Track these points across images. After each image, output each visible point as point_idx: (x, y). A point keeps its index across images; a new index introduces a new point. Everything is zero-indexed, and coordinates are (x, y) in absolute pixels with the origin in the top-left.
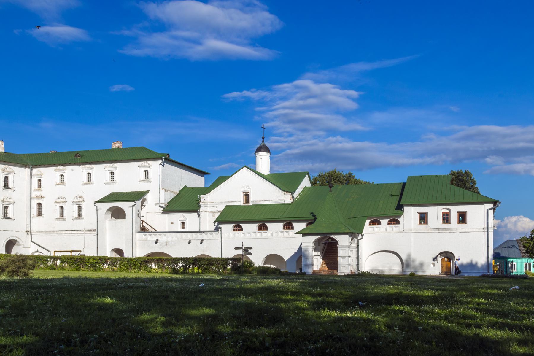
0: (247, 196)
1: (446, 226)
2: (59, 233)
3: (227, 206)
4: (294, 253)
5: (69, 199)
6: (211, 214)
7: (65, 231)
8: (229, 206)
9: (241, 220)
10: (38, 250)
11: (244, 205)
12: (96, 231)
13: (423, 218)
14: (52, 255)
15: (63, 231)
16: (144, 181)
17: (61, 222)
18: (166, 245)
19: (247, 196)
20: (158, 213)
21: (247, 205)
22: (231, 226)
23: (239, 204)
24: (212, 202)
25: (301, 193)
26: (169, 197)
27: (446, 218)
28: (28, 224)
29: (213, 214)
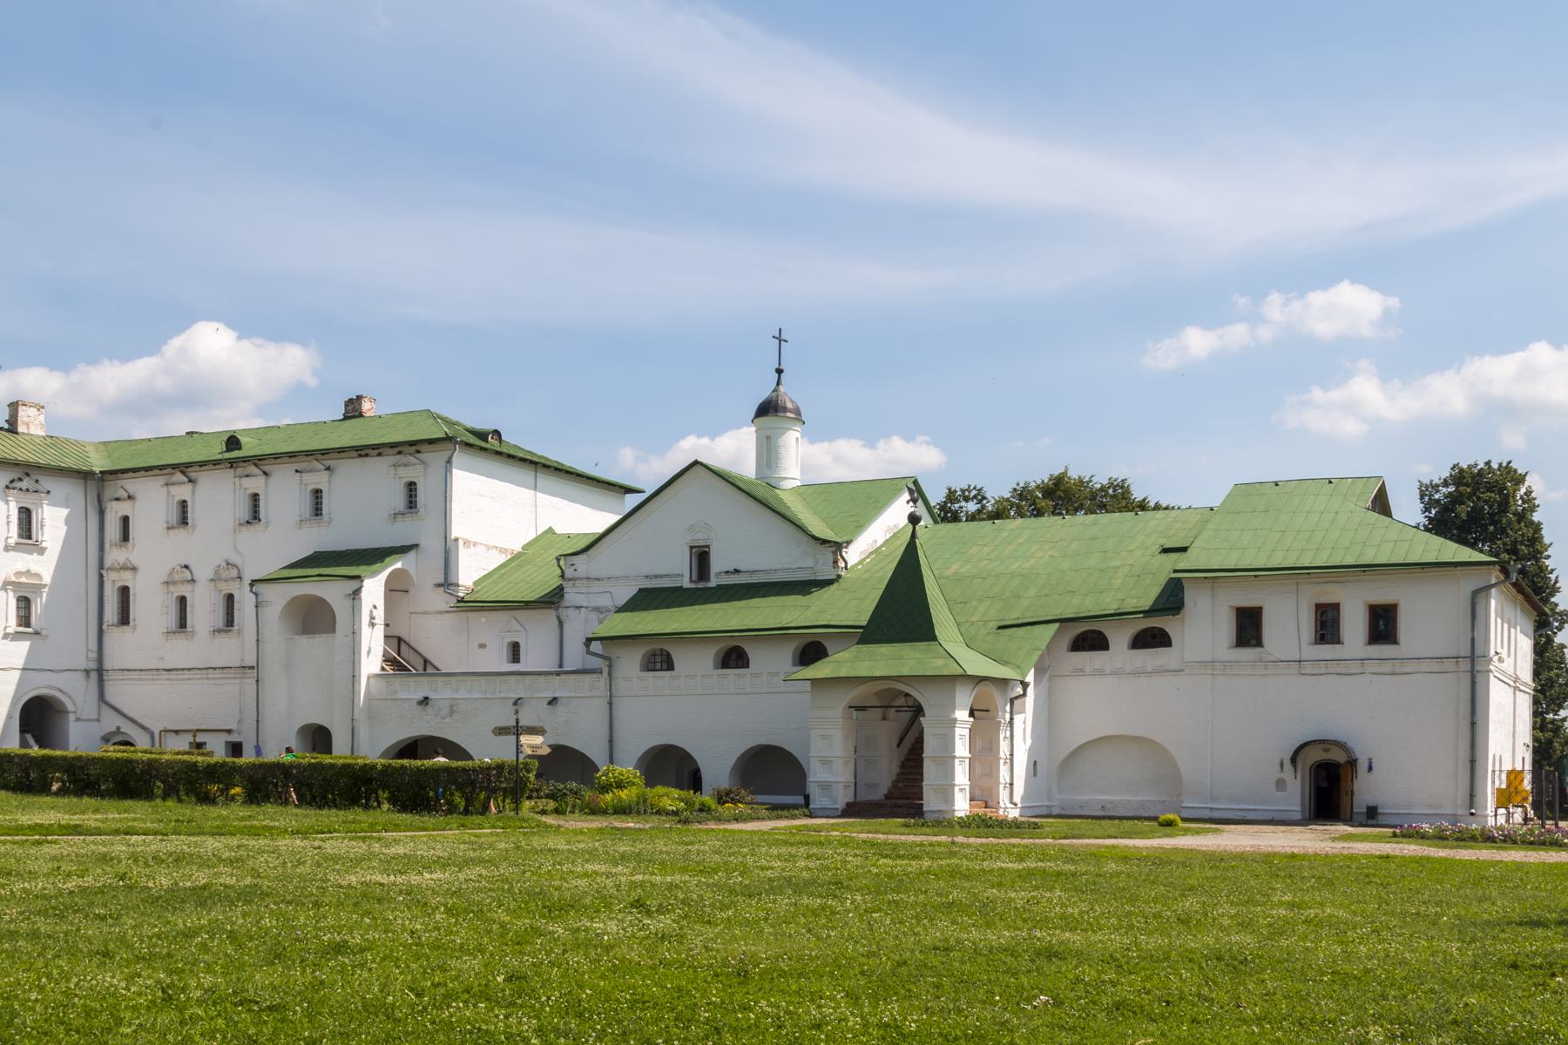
0: (701, 558)
1: (1326, 651)
2: (173, 675)
3: (641, 590)
5: (203, 572)
7: (189, 669)
8: (670, 588)
10: (118, 728)
11: (693, 586)
12: (255, 671)
13: (1249, 627)
15: (183, 669)
16: (403, 514)
17: (179, 642)
18: (452, 712)
20: (440, 612)
21: (700, 585)
23: (679, 585)
25: (882, 546)
26: (1308, 562)
27: (1327, 625)
28: (91, 651)
29: (601, 616)
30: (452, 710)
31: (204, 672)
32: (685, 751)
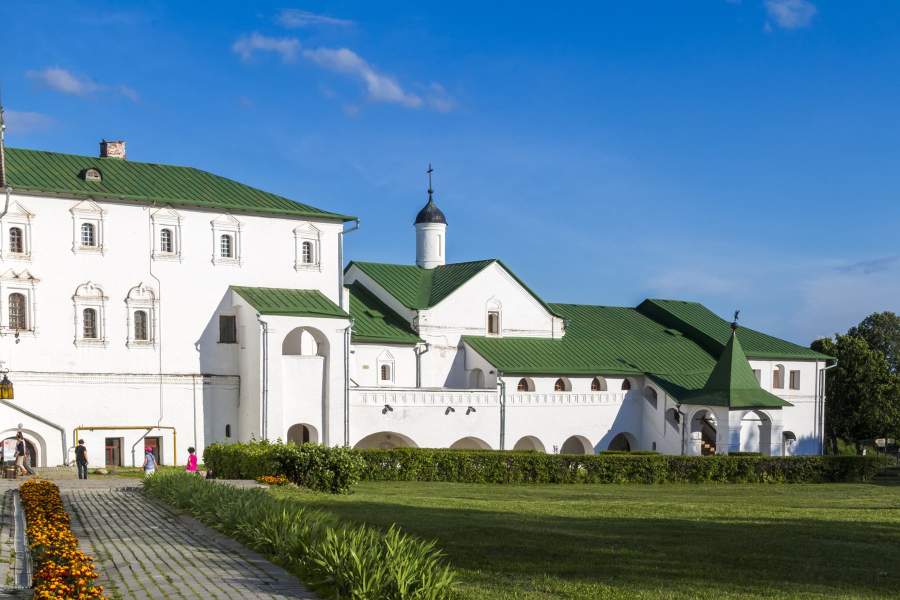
0: (493, 320)
2: (86, 379)
4: (607, 432)
5: (116, 295)
6: (438, 350)
9: (520, 370)
14: (332, 445)
18: (405, 416)
19: (493, 320)
22: (517, 380)
23: (483, 335)
24: (439, 327)
29: (442, 352)
30: (405, 414)
31: (123, 377)
32: (294, 426)
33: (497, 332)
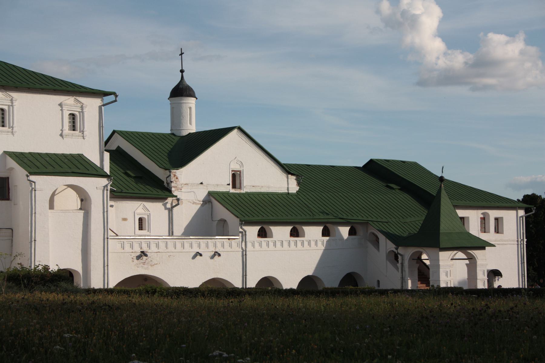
0: (236, 178)
33: (240, 188)
